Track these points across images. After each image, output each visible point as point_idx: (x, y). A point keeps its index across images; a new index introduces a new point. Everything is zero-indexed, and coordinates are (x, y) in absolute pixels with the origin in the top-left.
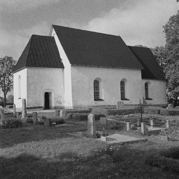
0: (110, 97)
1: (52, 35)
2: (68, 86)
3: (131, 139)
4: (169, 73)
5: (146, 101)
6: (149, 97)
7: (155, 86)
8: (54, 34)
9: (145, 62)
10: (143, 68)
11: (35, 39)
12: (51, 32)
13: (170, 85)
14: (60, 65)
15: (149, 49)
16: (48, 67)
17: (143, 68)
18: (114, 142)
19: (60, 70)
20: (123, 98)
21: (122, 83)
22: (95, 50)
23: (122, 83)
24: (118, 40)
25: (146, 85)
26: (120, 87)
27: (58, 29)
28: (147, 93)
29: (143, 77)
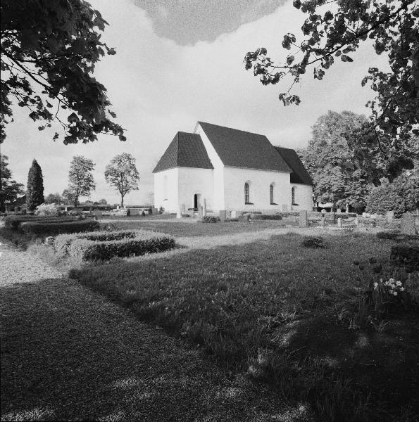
0: (261, 204)
1: (197, 133)
2: (221, 187)
3: (198, 241)
4: (316, 177)
5: (294, 207)
6: (295, 203)
7: (303, 191)
8: (200, 132)
9: (292, 165)
10: (292, 172)
11: (181, 136)
12: (196, 129)
13: (318, 191)
14: (208, 165)
15: (293, 151)
16: (195, 167)
17: (292, 172)
18: (81, 234)
19: (210, 170)
20: (247, 203)
21: (247, 185)
22: (245, 150)
23: (247, 185)
24: (262, 140)
25: (293, 189)
26: (271, 190)
27: (205, 126)
28: (247, 196)
29: (293, 181)
